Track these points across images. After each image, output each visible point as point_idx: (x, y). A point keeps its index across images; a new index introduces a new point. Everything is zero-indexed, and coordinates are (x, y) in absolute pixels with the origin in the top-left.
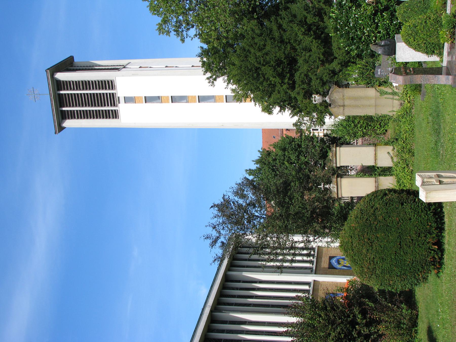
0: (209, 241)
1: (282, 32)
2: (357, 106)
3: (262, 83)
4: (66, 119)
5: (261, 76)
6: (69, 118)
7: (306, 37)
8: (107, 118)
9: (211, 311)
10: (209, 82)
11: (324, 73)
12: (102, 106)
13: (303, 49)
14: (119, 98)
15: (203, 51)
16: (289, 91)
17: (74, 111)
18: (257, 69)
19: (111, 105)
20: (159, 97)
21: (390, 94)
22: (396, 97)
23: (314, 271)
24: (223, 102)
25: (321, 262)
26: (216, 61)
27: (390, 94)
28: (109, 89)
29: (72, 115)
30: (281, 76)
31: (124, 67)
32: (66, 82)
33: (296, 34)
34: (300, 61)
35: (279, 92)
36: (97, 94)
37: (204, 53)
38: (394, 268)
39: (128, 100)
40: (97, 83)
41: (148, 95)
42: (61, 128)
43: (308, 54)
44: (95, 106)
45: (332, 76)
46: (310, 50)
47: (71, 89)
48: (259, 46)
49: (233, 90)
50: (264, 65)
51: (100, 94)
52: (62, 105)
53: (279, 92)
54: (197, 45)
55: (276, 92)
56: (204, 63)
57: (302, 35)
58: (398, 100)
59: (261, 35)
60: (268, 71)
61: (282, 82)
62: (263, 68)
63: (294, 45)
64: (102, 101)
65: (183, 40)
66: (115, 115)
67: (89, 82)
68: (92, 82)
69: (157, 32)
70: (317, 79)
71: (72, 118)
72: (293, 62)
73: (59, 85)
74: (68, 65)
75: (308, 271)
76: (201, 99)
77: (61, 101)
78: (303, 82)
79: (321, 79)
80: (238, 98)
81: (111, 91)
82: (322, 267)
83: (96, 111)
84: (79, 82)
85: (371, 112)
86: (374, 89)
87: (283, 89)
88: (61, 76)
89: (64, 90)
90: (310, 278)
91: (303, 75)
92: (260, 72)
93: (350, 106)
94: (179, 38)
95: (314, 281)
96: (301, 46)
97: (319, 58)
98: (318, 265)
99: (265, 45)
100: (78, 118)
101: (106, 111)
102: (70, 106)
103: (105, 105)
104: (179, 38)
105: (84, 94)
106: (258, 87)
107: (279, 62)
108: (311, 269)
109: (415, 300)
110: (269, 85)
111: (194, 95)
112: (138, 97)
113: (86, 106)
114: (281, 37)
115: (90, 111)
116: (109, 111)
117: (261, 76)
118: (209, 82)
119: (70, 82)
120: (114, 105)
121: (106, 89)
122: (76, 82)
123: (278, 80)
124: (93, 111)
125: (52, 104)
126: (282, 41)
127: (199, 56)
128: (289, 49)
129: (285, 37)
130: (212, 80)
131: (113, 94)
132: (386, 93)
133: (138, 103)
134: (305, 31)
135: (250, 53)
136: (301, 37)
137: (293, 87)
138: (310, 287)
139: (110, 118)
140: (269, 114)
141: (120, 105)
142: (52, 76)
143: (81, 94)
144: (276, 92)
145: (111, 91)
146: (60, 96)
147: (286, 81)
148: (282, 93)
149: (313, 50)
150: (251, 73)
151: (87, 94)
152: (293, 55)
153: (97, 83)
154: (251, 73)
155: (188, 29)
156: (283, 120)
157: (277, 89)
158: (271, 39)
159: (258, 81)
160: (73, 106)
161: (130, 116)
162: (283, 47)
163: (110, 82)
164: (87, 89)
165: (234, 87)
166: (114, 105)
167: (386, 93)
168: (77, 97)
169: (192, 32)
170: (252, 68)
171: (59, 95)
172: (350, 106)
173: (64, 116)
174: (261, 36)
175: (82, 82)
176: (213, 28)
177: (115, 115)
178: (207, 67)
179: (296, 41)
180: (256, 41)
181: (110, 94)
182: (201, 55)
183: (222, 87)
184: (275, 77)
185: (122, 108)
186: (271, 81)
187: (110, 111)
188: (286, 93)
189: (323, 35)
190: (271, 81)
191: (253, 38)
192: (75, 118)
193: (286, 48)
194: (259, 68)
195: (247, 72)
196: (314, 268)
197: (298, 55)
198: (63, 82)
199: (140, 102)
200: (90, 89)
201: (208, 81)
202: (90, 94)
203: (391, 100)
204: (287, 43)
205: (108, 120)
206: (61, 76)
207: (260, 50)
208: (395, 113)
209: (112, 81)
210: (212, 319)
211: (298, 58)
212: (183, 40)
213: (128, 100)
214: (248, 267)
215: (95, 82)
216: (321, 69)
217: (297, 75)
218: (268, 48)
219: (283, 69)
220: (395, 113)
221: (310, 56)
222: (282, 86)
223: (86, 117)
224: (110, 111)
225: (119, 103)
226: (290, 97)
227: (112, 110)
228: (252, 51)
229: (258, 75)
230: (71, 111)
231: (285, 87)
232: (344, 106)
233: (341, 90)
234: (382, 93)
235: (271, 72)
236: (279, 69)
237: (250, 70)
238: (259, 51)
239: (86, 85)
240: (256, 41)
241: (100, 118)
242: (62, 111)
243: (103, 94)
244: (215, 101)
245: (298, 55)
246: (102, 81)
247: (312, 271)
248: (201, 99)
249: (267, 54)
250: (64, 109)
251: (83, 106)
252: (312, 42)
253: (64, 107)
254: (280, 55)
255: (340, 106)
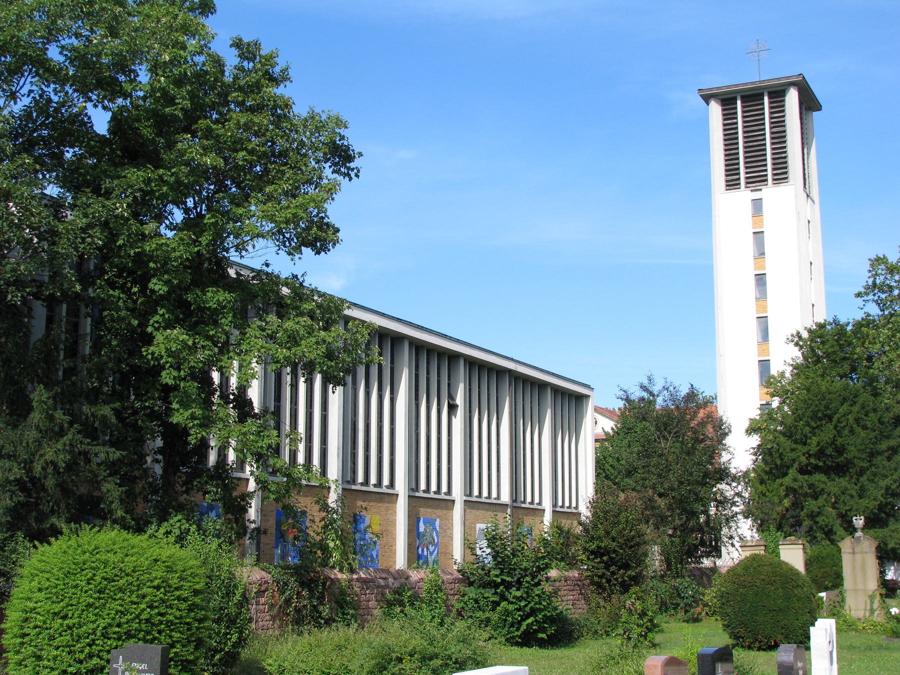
0: (646, 382)
1: (887, 454)
2: (854, 568)
3: (808, 424)
4: (723, 105)
5: (818, 423)
6: (723, 110)
7: (883, 491)
8: (726, 171)
9: (510, 371)
10: (792, 336)
11: (827, 517)
12: (746, 163)
13: (862, 486)
14: (761, 190)
15: (842, 326)
16: (796, 465)
17: (736, 118)
18: (830, 418)
19: (747, 178)
20: (763, 254)
21: (872, 606)
22: (867, 614)
23: (348, 487)
24: (759, 355)
25: (428, 507)
26: (828, 347)
27: (872, 606)
28: (774, 175)
29: (729, 115)
30: (821, 454)
31: (808, 196)
32: (784, 106)
33: (886, 477)
34: (843, 482)
35: (793, 450)
36: (765, 155)
37: (840, 329)
38: (748, 605)
39: (757, 205)
40: (783, 155)
41: (766, 235)
42: (707, 98)
43: (854, 494)
44: (745, 152)
45: (823, 529)
46: (861, 497)
47: (771, 113)
48: (863, 419)
49: (782, 374)
50: (836, 427)
51: (766, 160)
52: (745, 99)
53: (793, 450)
54: (852, 312)
55: (794, 446)
56: (821, 326)
57: (887, 486)
58: (865, 616)
59: (881, 423)
60: (827, 433)
61: (810, 456)
62: (832, 427)
63: (868, 472)
64: (754, 160)
65: (859, 295)
66: (732, 184)
67: (785, 142)
68: (785, 147)
69: (873, 257)
70: (819, 508)
71: (724, 115)
72: (841, 470)
73: (778, 94)
74: (809, 103)
75: (413, 485)
76: (763, 321)
77: (752, 97)
78: (811, 486)
79: (819, 514)
80: (767, 380)
81: (770, 177)
82: (421, 509)
83: (738, 154)
84: (784, 126)
85: (848, 583)
86: (876, 588)
87: (799, 457)
88: (792, 98)
89: (770, 103)
90: (401, 486)
91: (822, 486)
92: (824, 422)
93: (854, 560)
94: (863, 290)
95: (397, 495)
96: (866, 483)
97: (850, 510)
98: (422, 500)
99: (865, 428)
100: (724, 125)
101: (738, 169)
102: (743, 112)
103: (746, 168)
104: (863, 290)
105: (764, 134)
106: (801, 420)
107: (840, 450)
108: (354, 481)
109: (561, 647)
110: (806, 436)
111: (769, 309)
112: (762, 221)
113: (745, 137)
114: (880, 453)
115: (737, 143)
116: (739, 174)
117: (818, 423)
118: (792, 336)
119: (783, 111)
120: (747, 183)
121: (774, 169)
122: (784, 121)
123: (814, 449)
124: (738, 148)
125: (747, 84)
126: (872, 455)
127: (834, 320)
128: (861, 464)
129: (879, 458)
130: (797, 339)
131: (766, 180)
132: (872, 603)
133: (753, 221)
134: (893, 490)
135: (851, 405)
136: (883, 483)
137: (803, 471)
138: (387, 487)
139: (727, 175)
140: (747, 431)
141: (748, 192)
142: (793, 84)
143: (764, 129)
144: (794, 446)
145: (770, 177)
146: (760, 97)
147: (813, 461)
148: (793, 455)
149: (861, 501)
150: (822, 408)
151: (765, 139)
152: (851, 470)
153: (783, 155)
154: (822, 408)
155: (876, 302)
156: (740, 452)
157: (799, 447)
158: (876, 438)
159: (811, 418)
160: (744, 117)
161: (731, 207)
162: (863, 456)
163: (785, 176)
164: (772, 138)
165: (788, 375)
166: (747, 183)
167: (872, 603)
168: (757, 124)
169: (874, 310)
170: (830, 409)
171: (762, 95)
172: (854, 560)
173: (727, 101)
174: (880, 423)
175: (784, 131)
176: (887, 348)
177: (732, 184)
178: (819, 333)
179: (875, 475)
180: (872, 415)
181: (766, 175)
182: (836, 322)
183: (785, 357)
184: (818, 445)
185: (744, 196)
186: (810, 438)
187: (737, 177)
188: (794, 460)
189: (883, 515)
190: (810, 438)
191: (875, 410)
192: (724, 120)
193: (863, 460)
194: (831, 421)
195: (823, 403)
196: (354, 487)
197: (851, 477)
198: (783, 101)
199: (755, 224)
200: (773, 144)
201: (795, 333)
202: (765, 145)
203: (863, 607)
204: (870, 461)
205: (723, 173)
206: (792, 98)
207: (857, 420)
208: (848, 612)
209: (786, 178)
210: (453, 357)
211: (847, 478)
212: (859, 295)
213: (757, 205)
214: (417, 376)
215: (785, 152)
216: (834, 512)
217: (821, 477)
218: (863, 434)
219: (831, 456)
220: (848, 612)
221: (852, 497)
222: (804, 455)
223: (727, 137)
224: (737, 177)
225: (752, 191)
226: (788, 467)
227: (739, 179)
228: (855, 408)
229: (820, 419)
230: (736, 113)
231: (803, 459)
232: (854, 553)
233: (874, 549)
234: (872, 598)
235: (826, 439)
236: (830, 449)
237: (827, 407)
238: (855, 419)
239: (780, 138)
240: (872, 415)
241: (726, 160)
242: (735, 99)
243: (766, 165)
244: (759, 344)
245: (851, 477)
246: (786, 163)
247: (348, 482)
248: (763, 321)
249: (852, 431)
250: (739, 102)
251: (744, 132)
252: (875, 499)
253: (742, 102)
254: (852, 452)
255: (853, 549)
